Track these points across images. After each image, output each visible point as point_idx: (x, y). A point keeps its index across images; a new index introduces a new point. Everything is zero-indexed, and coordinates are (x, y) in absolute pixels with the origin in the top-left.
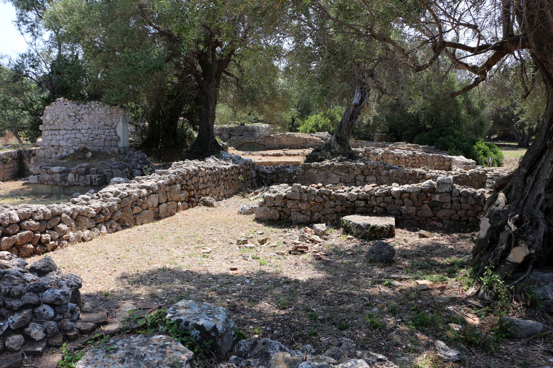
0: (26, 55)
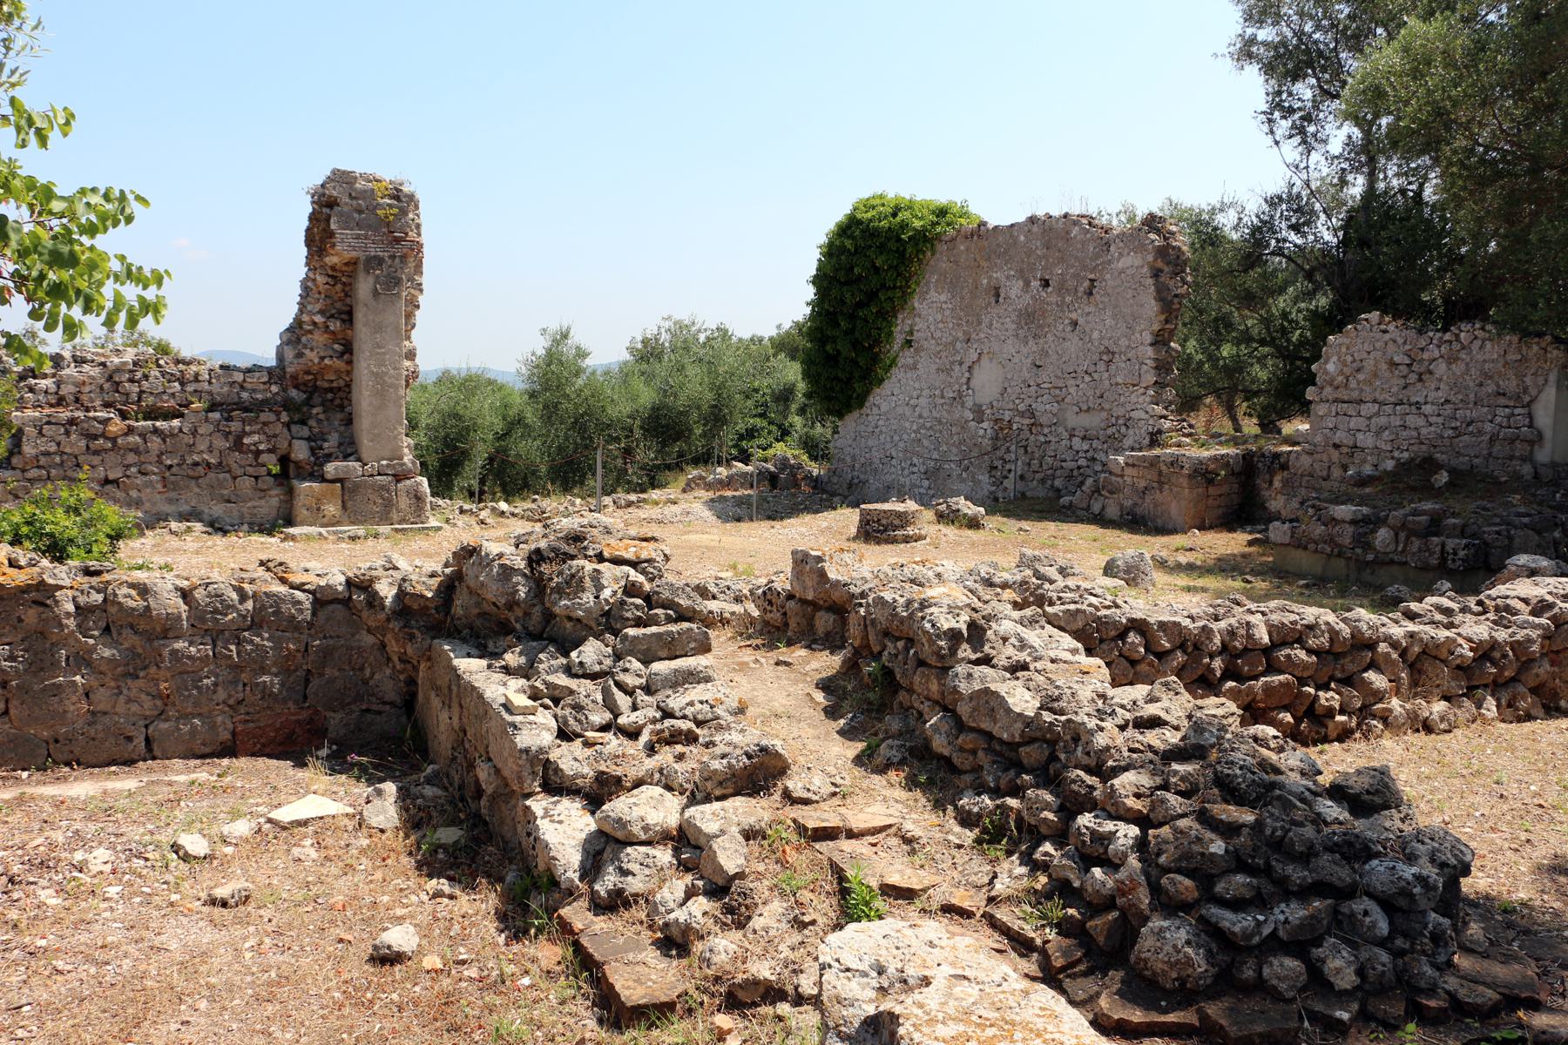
0: (1280, 198)
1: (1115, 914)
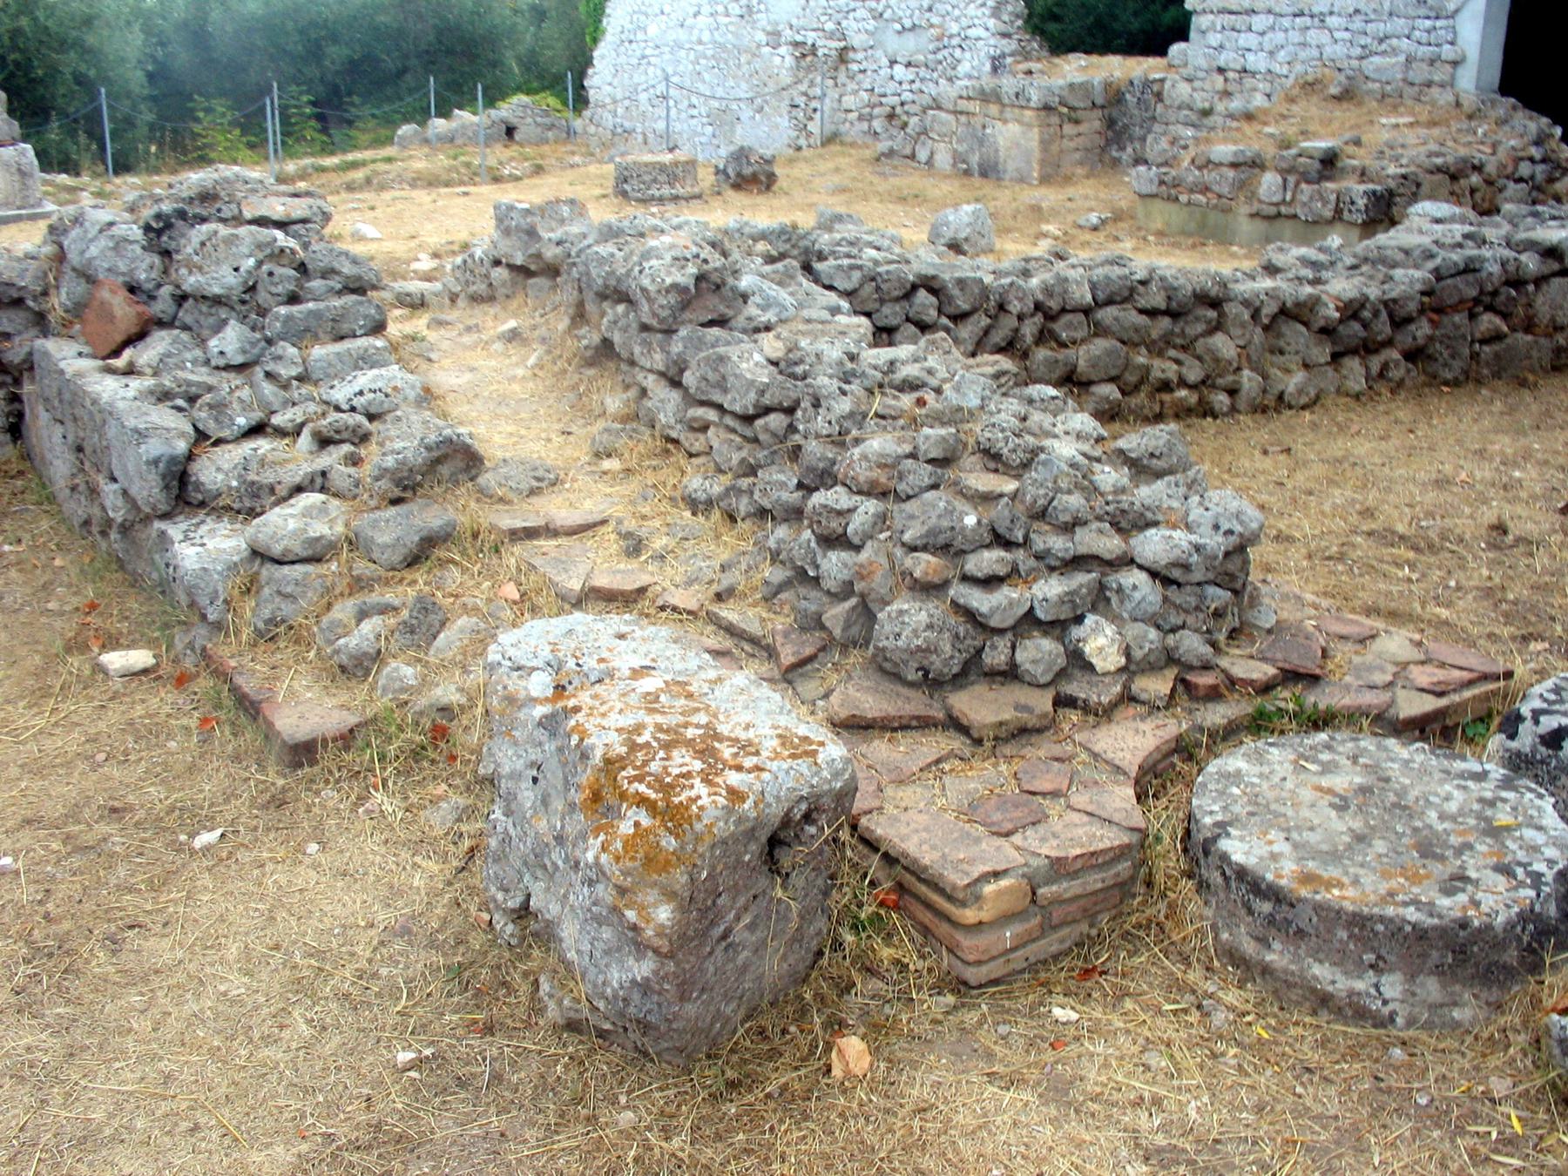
1: (853, 601)
